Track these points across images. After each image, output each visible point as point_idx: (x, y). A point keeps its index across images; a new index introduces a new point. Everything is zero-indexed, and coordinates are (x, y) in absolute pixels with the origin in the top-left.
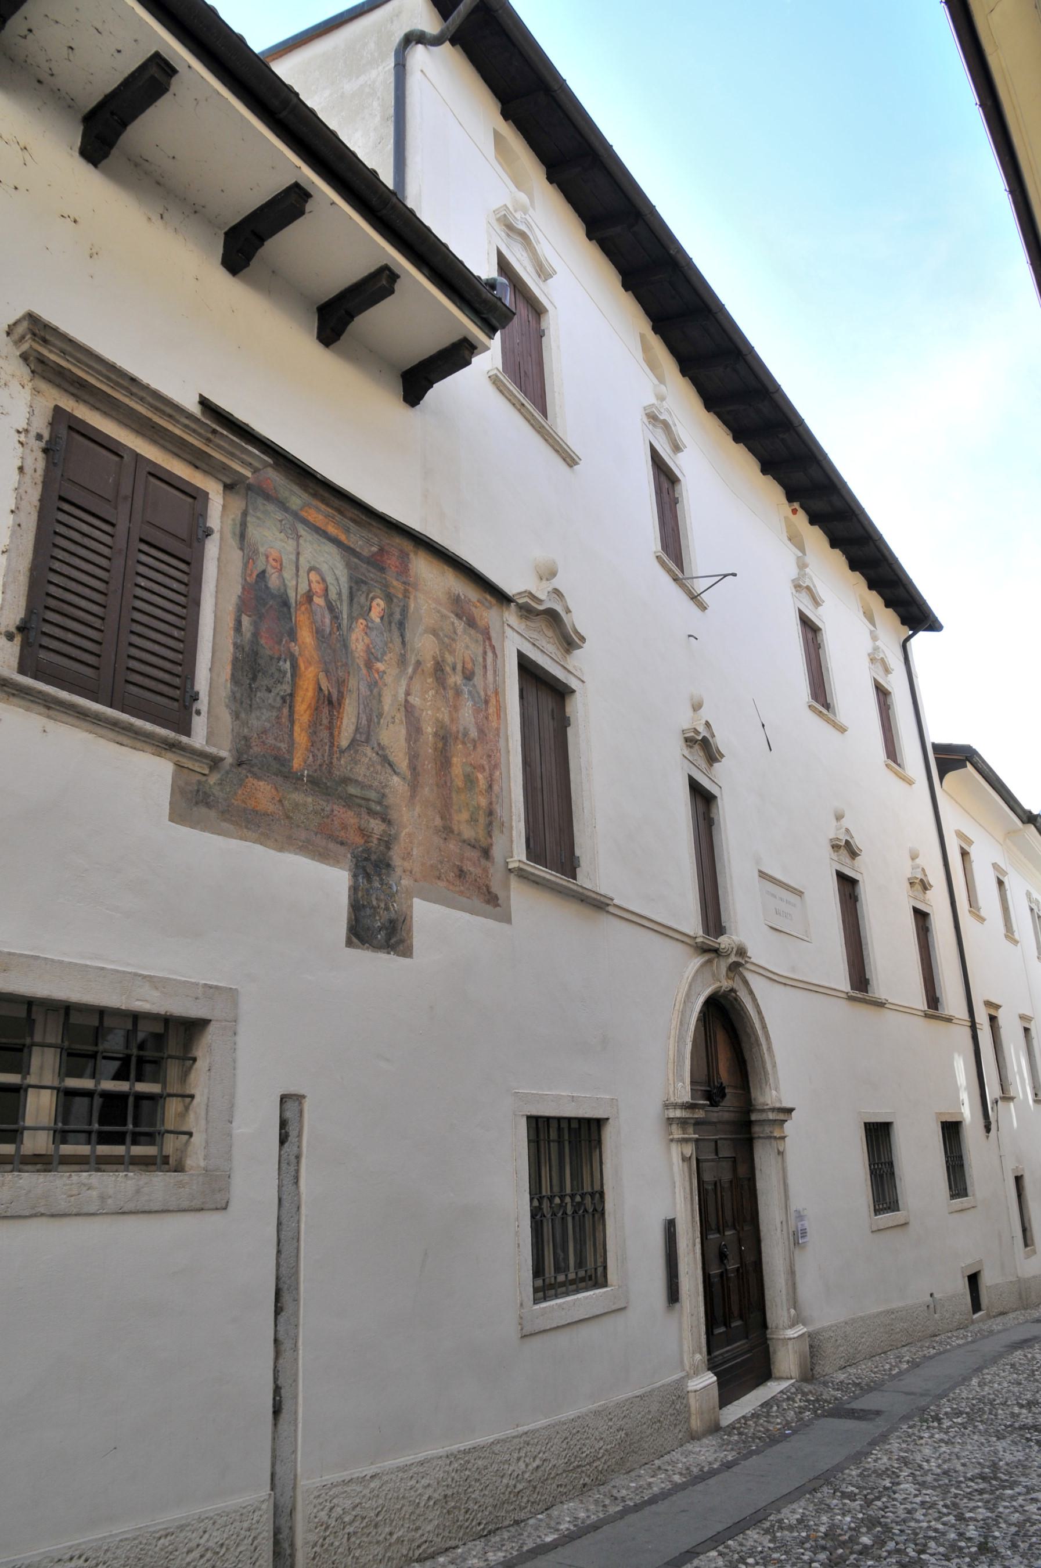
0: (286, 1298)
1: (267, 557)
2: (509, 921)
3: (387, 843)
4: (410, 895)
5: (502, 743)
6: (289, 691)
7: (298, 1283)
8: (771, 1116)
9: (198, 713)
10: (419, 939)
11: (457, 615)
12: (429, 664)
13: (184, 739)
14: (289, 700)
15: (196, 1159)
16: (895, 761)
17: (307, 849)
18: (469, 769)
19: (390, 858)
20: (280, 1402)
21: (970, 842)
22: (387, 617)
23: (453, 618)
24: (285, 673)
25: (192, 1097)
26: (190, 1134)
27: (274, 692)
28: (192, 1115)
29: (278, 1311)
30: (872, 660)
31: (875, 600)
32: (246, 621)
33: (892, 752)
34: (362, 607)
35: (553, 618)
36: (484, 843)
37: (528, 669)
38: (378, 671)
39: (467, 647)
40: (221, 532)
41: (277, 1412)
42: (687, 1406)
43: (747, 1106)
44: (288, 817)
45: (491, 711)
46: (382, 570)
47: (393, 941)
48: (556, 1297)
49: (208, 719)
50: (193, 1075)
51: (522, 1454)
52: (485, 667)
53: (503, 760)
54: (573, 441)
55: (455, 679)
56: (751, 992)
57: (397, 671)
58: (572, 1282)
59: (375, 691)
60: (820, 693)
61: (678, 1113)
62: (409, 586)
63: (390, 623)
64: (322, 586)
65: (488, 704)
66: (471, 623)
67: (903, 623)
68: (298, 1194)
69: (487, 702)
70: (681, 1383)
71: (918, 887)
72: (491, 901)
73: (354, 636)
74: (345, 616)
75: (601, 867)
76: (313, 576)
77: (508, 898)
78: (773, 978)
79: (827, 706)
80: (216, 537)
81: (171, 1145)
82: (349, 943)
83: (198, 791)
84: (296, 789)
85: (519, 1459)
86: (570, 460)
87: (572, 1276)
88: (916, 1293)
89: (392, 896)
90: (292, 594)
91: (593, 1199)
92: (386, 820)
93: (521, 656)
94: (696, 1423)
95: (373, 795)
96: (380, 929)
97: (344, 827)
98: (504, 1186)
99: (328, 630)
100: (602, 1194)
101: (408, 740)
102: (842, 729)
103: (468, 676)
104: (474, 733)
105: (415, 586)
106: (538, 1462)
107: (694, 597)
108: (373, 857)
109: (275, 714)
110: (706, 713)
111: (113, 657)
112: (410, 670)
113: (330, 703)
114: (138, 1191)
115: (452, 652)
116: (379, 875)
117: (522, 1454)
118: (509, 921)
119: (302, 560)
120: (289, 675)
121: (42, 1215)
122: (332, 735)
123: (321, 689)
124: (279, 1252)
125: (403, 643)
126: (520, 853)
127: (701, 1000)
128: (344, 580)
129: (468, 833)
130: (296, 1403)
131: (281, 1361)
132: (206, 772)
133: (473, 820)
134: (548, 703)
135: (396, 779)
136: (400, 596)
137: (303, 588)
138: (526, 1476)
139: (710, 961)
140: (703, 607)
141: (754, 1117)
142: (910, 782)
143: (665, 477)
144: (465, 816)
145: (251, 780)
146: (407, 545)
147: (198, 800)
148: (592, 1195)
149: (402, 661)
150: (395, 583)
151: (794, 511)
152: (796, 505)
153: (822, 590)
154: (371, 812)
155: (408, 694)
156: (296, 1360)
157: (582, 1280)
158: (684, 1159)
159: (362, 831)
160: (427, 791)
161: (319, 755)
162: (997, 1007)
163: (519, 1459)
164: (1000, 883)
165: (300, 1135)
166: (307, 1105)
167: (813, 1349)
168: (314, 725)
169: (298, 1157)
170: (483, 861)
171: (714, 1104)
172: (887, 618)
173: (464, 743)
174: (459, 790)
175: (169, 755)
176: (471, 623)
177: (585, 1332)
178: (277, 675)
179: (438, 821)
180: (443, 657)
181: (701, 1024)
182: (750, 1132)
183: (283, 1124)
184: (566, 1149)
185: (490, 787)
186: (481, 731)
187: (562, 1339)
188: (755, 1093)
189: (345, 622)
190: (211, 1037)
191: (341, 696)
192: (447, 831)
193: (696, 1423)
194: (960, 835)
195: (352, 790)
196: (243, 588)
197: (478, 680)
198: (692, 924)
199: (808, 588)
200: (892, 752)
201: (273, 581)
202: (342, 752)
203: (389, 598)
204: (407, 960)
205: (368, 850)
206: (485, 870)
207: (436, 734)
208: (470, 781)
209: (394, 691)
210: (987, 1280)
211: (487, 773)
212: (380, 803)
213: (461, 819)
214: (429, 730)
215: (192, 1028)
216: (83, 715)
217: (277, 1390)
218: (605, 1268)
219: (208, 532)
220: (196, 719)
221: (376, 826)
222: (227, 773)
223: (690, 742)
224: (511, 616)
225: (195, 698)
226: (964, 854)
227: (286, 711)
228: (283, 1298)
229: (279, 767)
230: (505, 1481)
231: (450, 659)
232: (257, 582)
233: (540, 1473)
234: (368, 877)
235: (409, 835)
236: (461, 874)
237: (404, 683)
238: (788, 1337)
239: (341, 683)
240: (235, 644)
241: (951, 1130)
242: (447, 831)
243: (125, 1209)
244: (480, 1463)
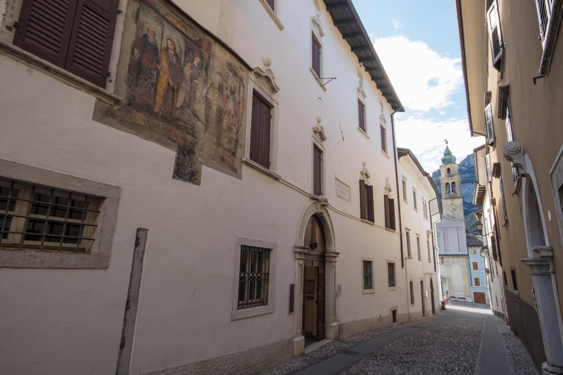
0: (131, 304)
1: (148, 29)
2: (241, 179)
3: (194, 144)
4: (201, 164)
5: (244, 118)
6: (155, 82)
7: (138, 298)
8: (332, 255)
9: (110, 81)
10: (203, 180)
11: (230, 70)
12: (217, 85)
13: (101, 89)
14: (155, 85)
15: (95, 250)
16: (385, 150)
17: (158, 140)
18: (229, 125)
19: (194, 150)
20: (124, 343)
21: (406, 179)
22: (201, 65)
23: (228, 71)
24: (153, 75)
25: (97, 226)
26: (94, 240)
27: (148, 81)
28: (96, 233)
29: (127, 308)
30: (381, 118)
31: (384, 100)
32: (136, 51)
33: (384, 148)
34: (190, 59)
35: (268, 79)
36: (233, 150)
37: (256, 94)
38: (195, 83)
39: (233, 82)
40: (126, 13)
41: (122, 346)
42: (293, 347)
43: (325, 251)
44: (150, 128)
45: (241, 106)
46: (200, 47)
47: (192, 179)
48: (247, 307)
49: (115, 84)
50: (98, 218)
51: (227, 362)
52: (240, 91)
53: (244, 124)
54: (282, 21)
55: (227, 92)
56: (329, 215)
57: (203, 85)
58: (254, 303)
59: (193, 90)
60: (362, 125)
61: (299, 250)
62: (211, 56)
63: (202, 67)
64: (173, 47)
65: (240, 104)
66: (235, 74)
67: (392, 108)
68: (142, 266)
69: (239, 103)
70: (292, 339)
71: (388, 190)
72: (235, 171)
73: (186, 69)
74: (183, 60)
75: (279, 165)
76: (169, 42)
77: (241, 171)
78: (336, 211)
79: (364, 130)
80: (124, 14)
81: (84, 244)
82: (174, 177)
83: (108, 111)
84: (155, 119)
85: (226, 364)
86: (281, 28)
87: (254, 301)
88: (375, 314)
89: (194, 163)
90: (159, 47)
91: (265, 275)
92: (193, 136)
93: (254, 90)
94: (296, 353)
95: (189, 127)
96: (188, 174)
97: (176, 136)
98: (230, 269)
99: (174, 63)
100: (268, 274)
101: (206, 110)
102: (368, 138)
103: (233, 93)
104: (233, 113)
105: (213, 56)
106: (233, 365)
107: (322, 86)
108: (187, 148)
109: (148, 89)
110: (322, 124)
111: (67, 49)
112: (209, 85)
113: (173, 90)
114: (62, 260)
115: (227, 83)
116: (189, 155)
117: (227, 362)
118: (241, 179)
119: (164, 35)
120: (155, 76)
121: (8, 267)
122: (173, 102)
123: (169, 84)
124: (130, 286)
125: (207, 75)
126: (247, 156)
127: (311, 215)
128: (183, 47)
129: (227, 146)
130: (132, 344)
131: (126, 327)
132: (113, 104)
133: (230, 142)
134: (264, 109)
135: (199, 122)
136: (207, 58)
137: (164, 45)
138: (228, 370)
139: (315, 203)
140: (325, 90)
141: (326, 255)
142: (389, 158)
143: (316, 46)
144: (226, 140)
145: (134, 112)
146: (212, 41)
147: (107, 113)
148: (265, 274)
149: (206, 82)
150: (205, 53)
151: (361, 66)
152: (362, 64)
153: (367, 93)
154: (187, 132)
155: (207, 93)
156: (134, 327)
157: (258, 302)
158: (299, 265)
159: (183, 138)
160: (211, 129)
161: (167, 108)
162: (409, 230)
163: (226, 364)
164: (414, 193)
165: (145, 244)
166: (149, 233)
167: (340, 328)
168: (165, 98)
169: (143, 252)
170: (232, 157)
171: (312, 249)
172: (387, 107)
173: (228, 115)
174: (225, 131)
175: (94, 94)
176: (235, 74)
177: (258, 319)
178: (150, 75)
179: (215, 140)
180: (223, 85)
181: (310, 223)
182: (325, 259)
183: (137, 239)
184: (254, 261)
185: (238, 132)
186: (236, 113)
187: (247, 322)
188: (327, 247)
189: (182, 62)
190: (105, 204)
191: (178, 89)
192: (219, 144)
193: (296, 353)
194: (402, 176)
195: (180, 123)
196: (136, 38)
197: (236, 95)
198: (310, 190)
199: (362, 91)
200: (384, 148)
201: (151, 39)
202: (177, 109)
203: (202, 58)
204: (198, 186)
205: (185, 146)
206: (233, 160)
207: (217, 110)
208: (230, 129)
209: (201, 91)
210: (399, 312)
211: (237, 127)
212: (192, 130)
213: (224, 141)
214: (215, 108)
215: (100, 200)
216: (47, 68)
217: (123, 338)
218: (267, 299)
219: (120, 12)
220: (108, 83)
221: (189, 138)
222: (123, 107)
223: (315, 132)
224: (252, 76)
225: (109, 75)
226: (404, 183)
227: (153, 89)
228: (130, 303)
229: (148, 109)
230: (219, 372)
231: (225, 85)
232: (143, 38)
233: (234, 369)
234: (184, 155)
235: (203, 143)
236: (223, 160)
237: (206, 90)
238: (332, 326)
239: (179, 85)
240: (131, 59)
241: (391, 266)
242: (219, 144)
243: (54, 267)
244: (209, 365)
